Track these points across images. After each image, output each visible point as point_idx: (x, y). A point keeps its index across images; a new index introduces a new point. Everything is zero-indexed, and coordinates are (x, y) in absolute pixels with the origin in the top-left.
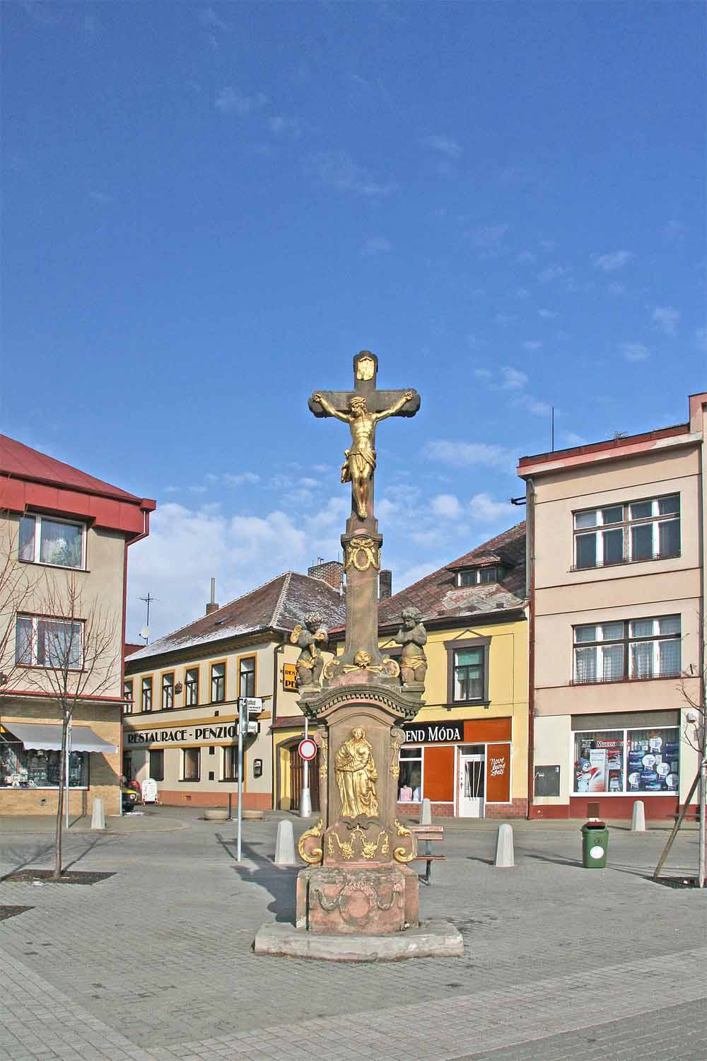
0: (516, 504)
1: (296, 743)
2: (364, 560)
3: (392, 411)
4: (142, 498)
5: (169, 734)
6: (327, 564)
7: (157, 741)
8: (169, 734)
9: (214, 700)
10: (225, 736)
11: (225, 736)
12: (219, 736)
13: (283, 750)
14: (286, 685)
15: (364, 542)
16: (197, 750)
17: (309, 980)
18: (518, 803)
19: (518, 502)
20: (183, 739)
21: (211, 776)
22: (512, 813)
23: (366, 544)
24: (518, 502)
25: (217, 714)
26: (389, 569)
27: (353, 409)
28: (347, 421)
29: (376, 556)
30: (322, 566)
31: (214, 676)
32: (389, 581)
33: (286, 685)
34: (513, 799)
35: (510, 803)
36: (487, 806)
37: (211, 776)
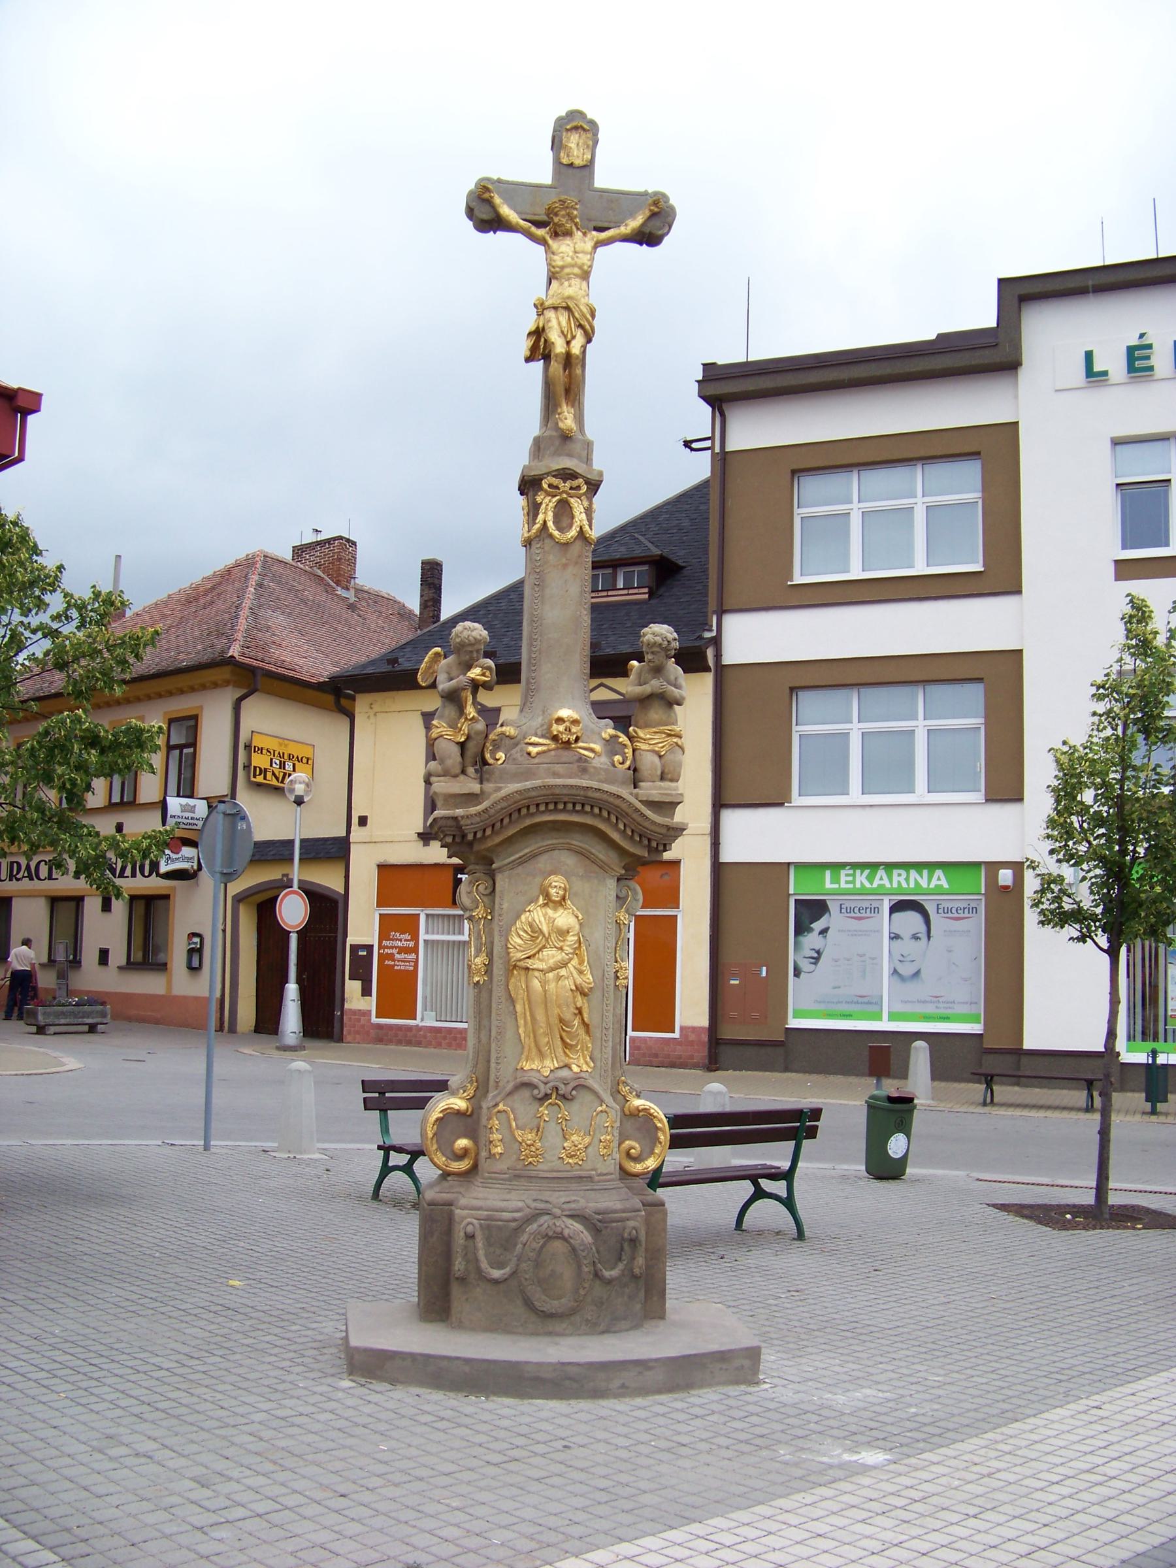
0: (692, 450)
1: (270, 894)
2: (565, 522)
3: (624, 230)
4: (16, 386)
5: (23, 868)
6: (329, 541)
7: (39, 879)
8: (23, 868)
9: (116, 799)
10: (134, 875)
11: (134, 875)
12: (122, 875)
13: (242, 909)
14: (255, 776)
15: (568, 484)
16: (79, 900)
17: (502, 1417)
18: (692, 1037)
19: (694, 445)
20: (50, 877)
21: (104, 956)
22: (680, 1057)
23: (571, 488)
24: (694, 445)
25: (119, 828)
26: (439, 558)
27: (556, 220)
28: (542, 242)
29: (589, 511)
30: (318, 543)
31: (172, 743)
32: (436, 581)
33: (255, 777)
34: (682, 1028)
35: (676, 1035)
36: (633, 1039)
37: (104, 956)
